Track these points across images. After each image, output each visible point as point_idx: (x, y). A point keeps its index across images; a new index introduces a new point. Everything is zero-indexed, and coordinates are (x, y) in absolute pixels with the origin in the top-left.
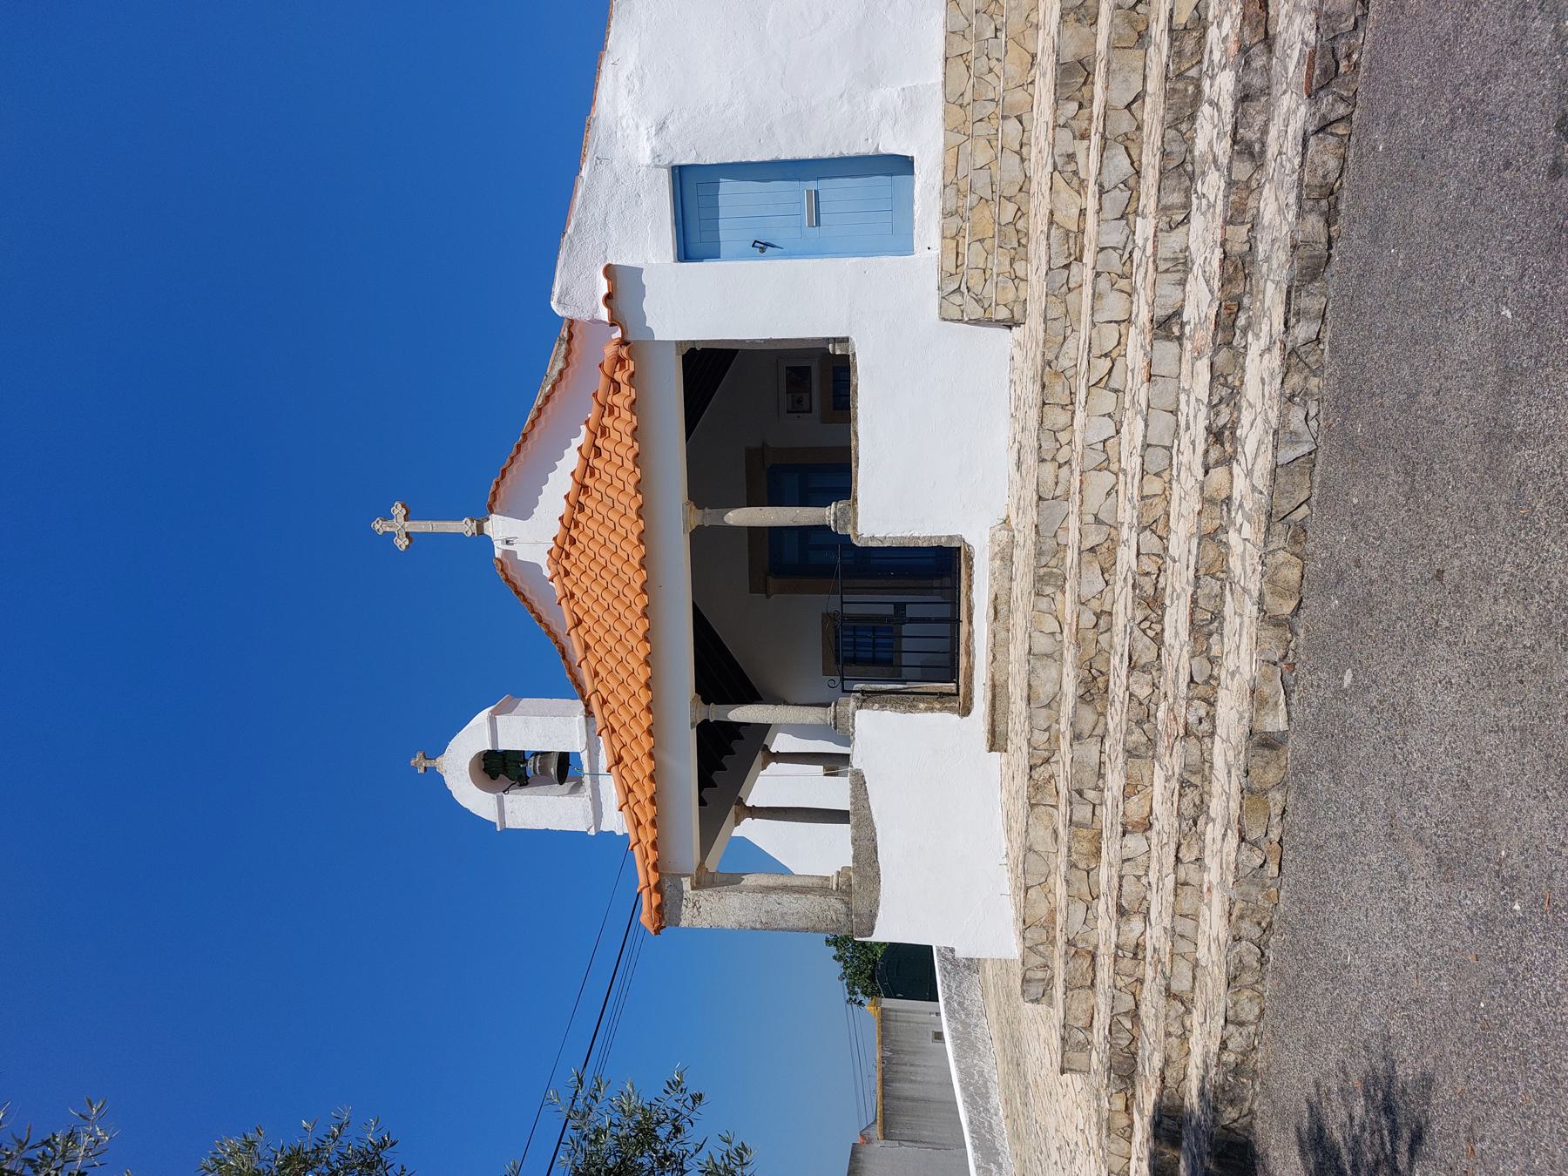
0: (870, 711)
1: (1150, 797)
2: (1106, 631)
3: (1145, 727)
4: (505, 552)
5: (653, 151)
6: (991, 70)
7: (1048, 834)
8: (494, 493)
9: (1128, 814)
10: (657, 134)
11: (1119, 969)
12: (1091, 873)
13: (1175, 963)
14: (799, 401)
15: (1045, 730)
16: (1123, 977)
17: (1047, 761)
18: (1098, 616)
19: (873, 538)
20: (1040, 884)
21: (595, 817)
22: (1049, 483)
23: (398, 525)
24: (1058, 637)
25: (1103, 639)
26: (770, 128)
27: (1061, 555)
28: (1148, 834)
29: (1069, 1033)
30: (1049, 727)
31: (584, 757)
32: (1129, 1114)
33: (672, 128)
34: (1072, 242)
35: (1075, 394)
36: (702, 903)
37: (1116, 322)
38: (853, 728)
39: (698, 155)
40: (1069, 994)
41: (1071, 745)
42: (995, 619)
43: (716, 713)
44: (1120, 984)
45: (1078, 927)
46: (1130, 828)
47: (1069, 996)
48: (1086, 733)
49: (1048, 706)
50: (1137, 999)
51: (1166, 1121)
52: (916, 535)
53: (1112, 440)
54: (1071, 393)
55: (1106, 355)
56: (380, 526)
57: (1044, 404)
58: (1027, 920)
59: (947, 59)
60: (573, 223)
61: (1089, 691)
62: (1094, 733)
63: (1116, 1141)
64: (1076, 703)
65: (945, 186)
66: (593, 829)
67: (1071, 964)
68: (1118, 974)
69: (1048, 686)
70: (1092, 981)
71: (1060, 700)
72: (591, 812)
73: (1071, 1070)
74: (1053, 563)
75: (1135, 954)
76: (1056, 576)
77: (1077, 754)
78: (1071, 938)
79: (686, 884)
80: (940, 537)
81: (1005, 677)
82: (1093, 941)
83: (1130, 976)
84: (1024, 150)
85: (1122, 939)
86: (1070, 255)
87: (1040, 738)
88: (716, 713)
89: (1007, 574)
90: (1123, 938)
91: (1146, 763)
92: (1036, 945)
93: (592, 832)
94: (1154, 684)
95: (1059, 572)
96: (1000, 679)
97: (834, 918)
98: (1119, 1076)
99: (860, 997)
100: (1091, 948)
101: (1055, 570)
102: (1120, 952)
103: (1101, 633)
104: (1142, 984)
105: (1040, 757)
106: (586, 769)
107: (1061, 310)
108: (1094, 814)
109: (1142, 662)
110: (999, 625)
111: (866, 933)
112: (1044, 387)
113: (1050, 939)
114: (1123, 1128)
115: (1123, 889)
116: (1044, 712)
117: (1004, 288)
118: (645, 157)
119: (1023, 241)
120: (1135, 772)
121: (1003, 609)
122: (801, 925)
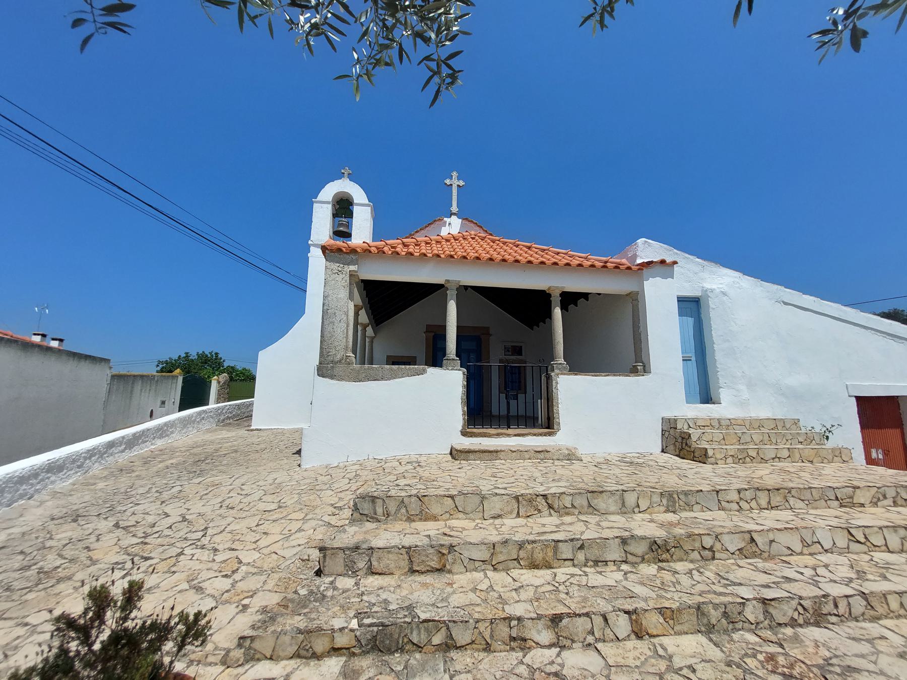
0: (462, 379)
1: (665, 633)
2: (701, 556)
3: (723, 621)
4: (446, 222)
5: (714, 289)
6: (787, 440)
8: (472, 222)
9: (647, 614)
10: (721, 291)
11: (497, 624)
12: (515, 562)
14: (508, 351)
15: (572, 504)
16: (489, 629)
17: (550, 507)
18: (711, 549)
19: (557, 383)
20: (456, 507)
22: (728, 497)
23: (455, 182)
24: (636, 510)
25: (695, 555)
26: (728, 341)
27: (687, 508)
28: (633, 636)
29: (364, 553)
30: (575, 507)
32: (328, 652)
33: (725, 298)
34: (848, 500)
35: (778, 510)
37: (886, 542)
38: (452, 370)
39: (713, 309)
40: (403, 551)
41: (617, 537)
42: (536, 452)
43: (452, 294)
44: (482, 626)
45: (466, 554)
46: (634, 617)
47: (401, 551)
48: (628, 548)
49: (590, 506)
50: (467, 647)
52: (560, 406)
53: (820, 547)
54: (777, 507)
55: (866, 538)
56: (455, 174)
57: (769, 490)
59: (775, 419)
60: (678, 252)
61: (659, 547)
62: (628, 555)
63: (293, 641)
64: (650, 538)
65: (729, 419)
66: (312, 243)
67: (431, 551)
68: (492, 623)
69: (604, 505)
70: (418, 571)
71: (595, 514)
73: (324, 557)
74: (681, 503)
75: (514, 639)
76: (674, 506)
77: (611, 542)
78: (455, 548)
79: (352, 268)
80: (559, 418)
81: (502, 458)
82: (457, 568)
83: (492, 636)
84: (777, 459)
85: (529, 623)
86: (842, 500)
87: (567, 501)
88: (452, 294)
91: (693, 626)
92: (405, 507)
93: (310, 242)
94: (758, 623)
95: (677, 507)
96: (501, 455)
97: (330, 354)
98: (376, 636)
99: (161, 366)
100: (448, 567)
101: (677, 505)
102: (514, 623)
103: (699, 553)
104: (485, 650)
105: (553, 502)
107: (816, 497)
108: (565, 560)
109: (771, 610)
110: (532, 454)
111: (320, 373)
112: (778, 490)
113: (412, 517)
114: (311, 647)
115: (577, 619)
116: (585, 503)
117: (721, 452)
118: (707, 286)
119: (741, 461)
120: (685, 617)
121: (541, 456)
122: (325, 333)
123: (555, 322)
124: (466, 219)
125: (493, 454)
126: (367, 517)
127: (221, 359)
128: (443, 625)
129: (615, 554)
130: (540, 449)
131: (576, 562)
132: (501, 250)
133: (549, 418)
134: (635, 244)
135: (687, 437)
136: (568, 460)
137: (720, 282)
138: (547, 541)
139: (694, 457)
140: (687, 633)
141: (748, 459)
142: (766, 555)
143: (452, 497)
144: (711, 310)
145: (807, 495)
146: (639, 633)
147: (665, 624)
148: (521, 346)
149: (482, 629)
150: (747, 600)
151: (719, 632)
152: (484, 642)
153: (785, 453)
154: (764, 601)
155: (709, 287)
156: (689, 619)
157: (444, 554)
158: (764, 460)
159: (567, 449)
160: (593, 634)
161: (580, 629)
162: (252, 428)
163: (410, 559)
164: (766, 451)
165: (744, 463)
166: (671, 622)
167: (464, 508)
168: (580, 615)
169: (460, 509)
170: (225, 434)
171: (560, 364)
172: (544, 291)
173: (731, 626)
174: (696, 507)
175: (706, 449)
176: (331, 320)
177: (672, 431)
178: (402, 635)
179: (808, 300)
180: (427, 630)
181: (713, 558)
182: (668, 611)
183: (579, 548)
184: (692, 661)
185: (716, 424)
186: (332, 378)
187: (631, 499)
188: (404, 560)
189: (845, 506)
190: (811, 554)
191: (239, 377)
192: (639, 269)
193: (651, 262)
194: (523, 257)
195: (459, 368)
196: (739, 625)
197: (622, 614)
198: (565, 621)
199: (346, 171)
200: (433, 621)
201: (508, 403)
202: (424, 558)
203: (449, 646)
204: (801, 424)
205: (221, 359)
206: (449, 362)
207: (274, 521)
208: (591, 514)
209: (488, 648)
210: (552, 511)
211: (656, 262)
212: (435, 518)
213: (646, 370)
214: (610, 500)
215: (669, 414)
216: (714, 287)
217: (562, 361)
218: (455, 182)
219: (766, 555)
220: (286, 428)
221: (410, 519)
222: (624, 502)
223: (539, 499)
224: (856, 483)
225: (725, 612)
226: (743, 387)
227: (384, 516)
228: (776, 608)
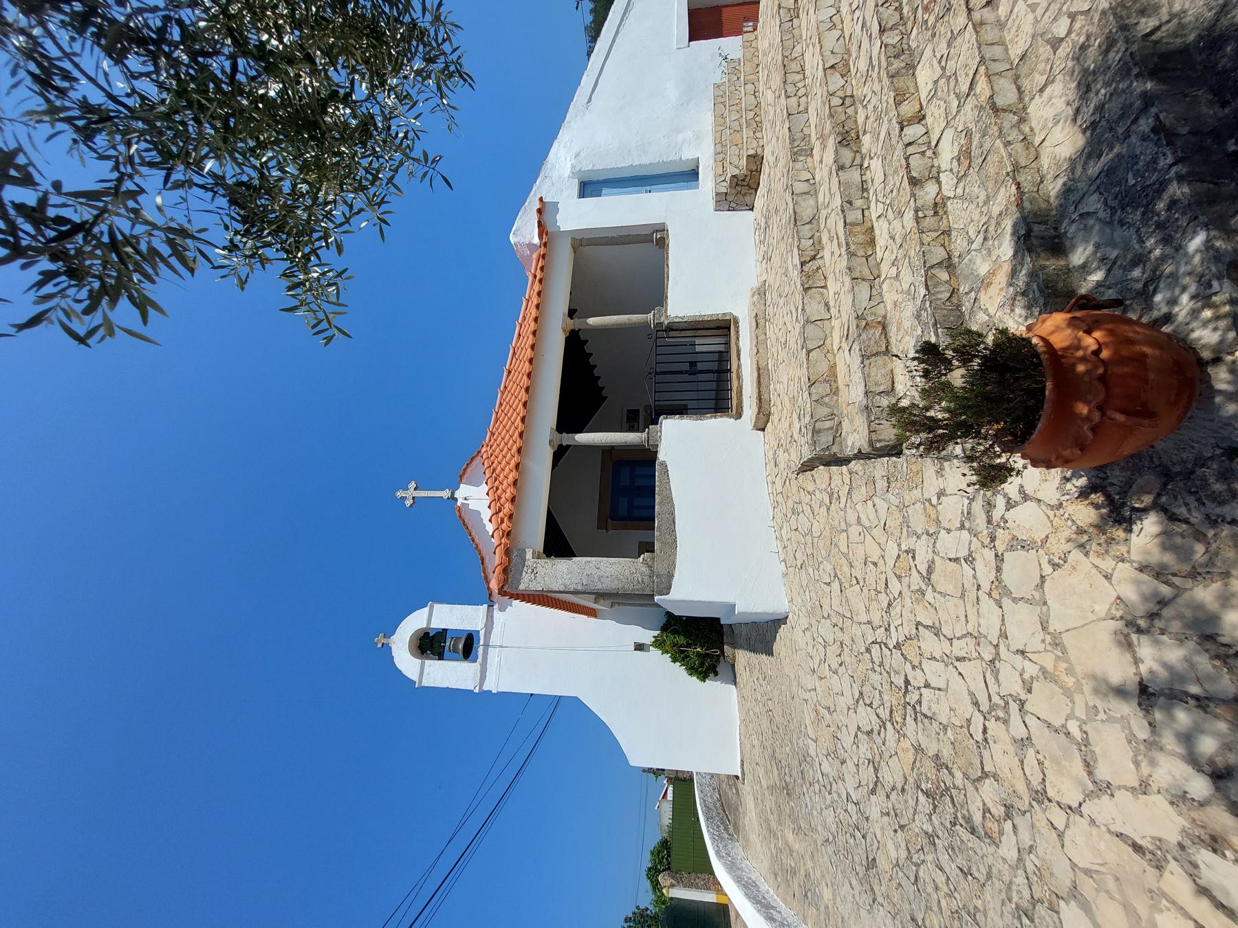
7: (822, 307)
8: (465, 470)
12: (869, 259)
13: (993, 83)
14: (633, 427)
17: (813, 258)
18: (844, 99)
20: (819, 347)
21: (480, 679)
25: (850, 111)
26: (629, 151)
28: (923, 122)
31: (482, 634)
33: (582, 154)
36: (539, 569)
43: (566, 439)
45: (865, 304)
46: (906, 123)
51: (1036, 228)
56: (400, 494)
58: (811, 377)
60: (528, 201)
67: (864, 336)
68: (923, 232)
70: (887, 347)
71: (819, 217)
72: (479, 675)
75: (936, 213)
76: (806, 150)
77: (842, 179)
79: (529, 555)
83: (935, 231)
85: (920, 203)
87: (806, 243)
88: (566, 439)
89: (763, 302)
90: (921, 201)
93: (477, 690)
96: (762, 364)
97: (640, 580)
100: (880, 319)
102: (920, 214)
104: (949, 235)
106: (482, 642)
108: (863, 216)
109: (890, 25)
110: (760, 331)
111: (665, 591)
112: (785, 66)
115: (911, 166)
118: (567, 172)
121: (761, 322)
123: (604, 323)
124: (461, 477)
125: (762, 376)
126: (836, 437)
127: (634, 913)
128: (929, 273)
129: (854, 175)
130: (754, 324)
131: (865, 207)
132: (500, 488)
133: (718, 328)
134: (516, 245)
135: (735, 180)
136: (765, 295)
137: (563, 159)
138: (845, 232)
139: (756, 171)
140: (916, 83)
141: (757, 119)
142: (845, 56)
143: (809, 352)
144: (595, 168)
145: (789, 44)
146: (920, 118)
147: (910, 99)
148: (628, 410)
149: (929, 239)
150: (882, 43)
151: (912, 61)
152: (942, 236)
153: (750, 87)
154: (882, 31)
155: (569, 170)
156: (901, 82)
157: (867, 324)
158: (758, 105)
159: (753, 296)
160: (924, 152)
161: (921, 162)
162: (740, 775)
163: (874, 355)
164: (748, 103)
165: (761, 122)
166: (907, 95)
167: (820, 340)
168: (908, 164)
169: (821, 343)
170: (753, 837)
171: (654, 316)
172: (554, 453)
173: (907, 52)
174: (806, 131)
175: (748, 156)
176: (596, 580)
177: (730, 198)
178: (943, 307)
179: (587, 81)
180: (937, 285)
181: (852, 96)
182: (897, 98)
183: (851, 205)
184: (935, 63)
185: (721, 156)
186: (673, 576)
187: (800, 187)
188: (876, 361)
189: (798, 14)
190: (842, 23)
191: (663, 858)
192: (547, 235)
193: (540, 224)
194: (511, 460)
195: (658, 426)
196: (905, 47)
197: (904, 133)
198: (914, 174)
199: (380, 640)
200: (926, 281)
201: (701, 372)
202: (872, 342)
203: (948, 264)
204: (719, 81)
205: (634, 913)
206: (651, 438)
207: (851, 566)
208: (819, 222)
209: (947, 233)
210: (818, 257)
211: (539, 218)
212: (833, 367)
213: (662, 228)
214: (803, 204)
215: (711, 205)
216: (569, 165)
217: (651, 315)
218: (410, 493)
219: (845, 56)
220: (737, 707)
221: (836, 392)
222: (805, 193)
223: (806, 268)
224: (776, 8)
225: (895, 57)
226: (680, 137)
227: (834, 419)
228: (887, 22)
